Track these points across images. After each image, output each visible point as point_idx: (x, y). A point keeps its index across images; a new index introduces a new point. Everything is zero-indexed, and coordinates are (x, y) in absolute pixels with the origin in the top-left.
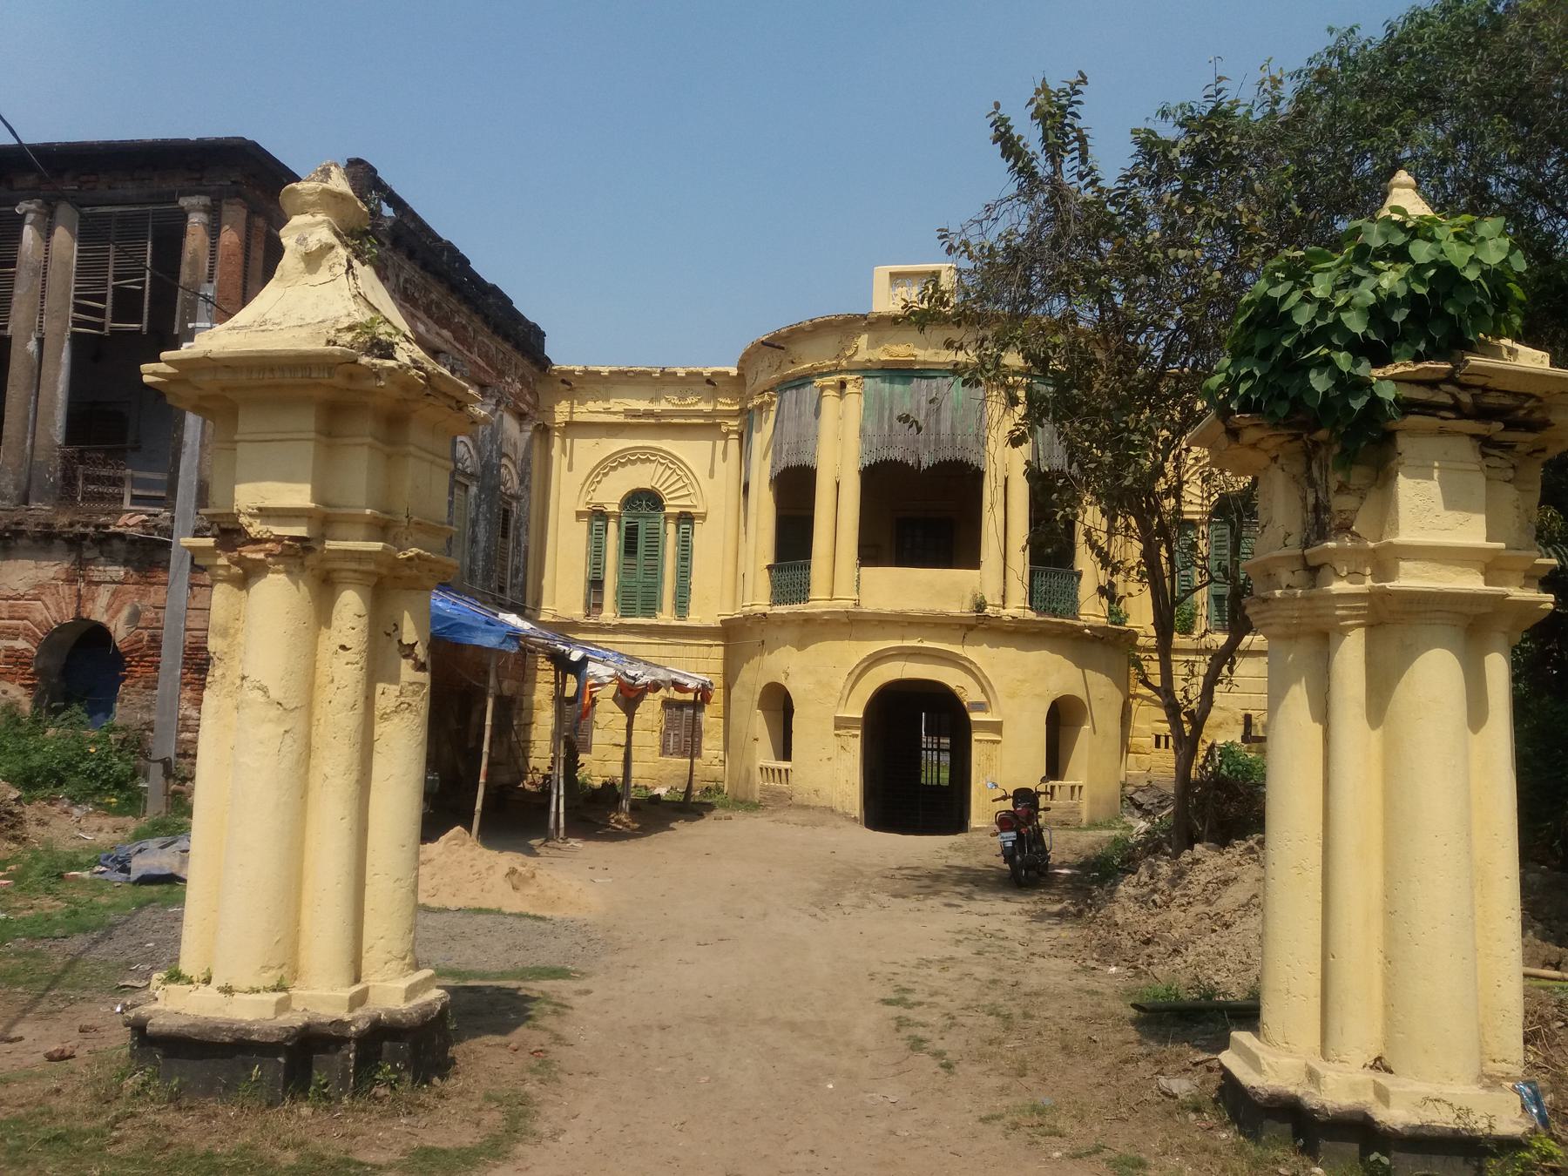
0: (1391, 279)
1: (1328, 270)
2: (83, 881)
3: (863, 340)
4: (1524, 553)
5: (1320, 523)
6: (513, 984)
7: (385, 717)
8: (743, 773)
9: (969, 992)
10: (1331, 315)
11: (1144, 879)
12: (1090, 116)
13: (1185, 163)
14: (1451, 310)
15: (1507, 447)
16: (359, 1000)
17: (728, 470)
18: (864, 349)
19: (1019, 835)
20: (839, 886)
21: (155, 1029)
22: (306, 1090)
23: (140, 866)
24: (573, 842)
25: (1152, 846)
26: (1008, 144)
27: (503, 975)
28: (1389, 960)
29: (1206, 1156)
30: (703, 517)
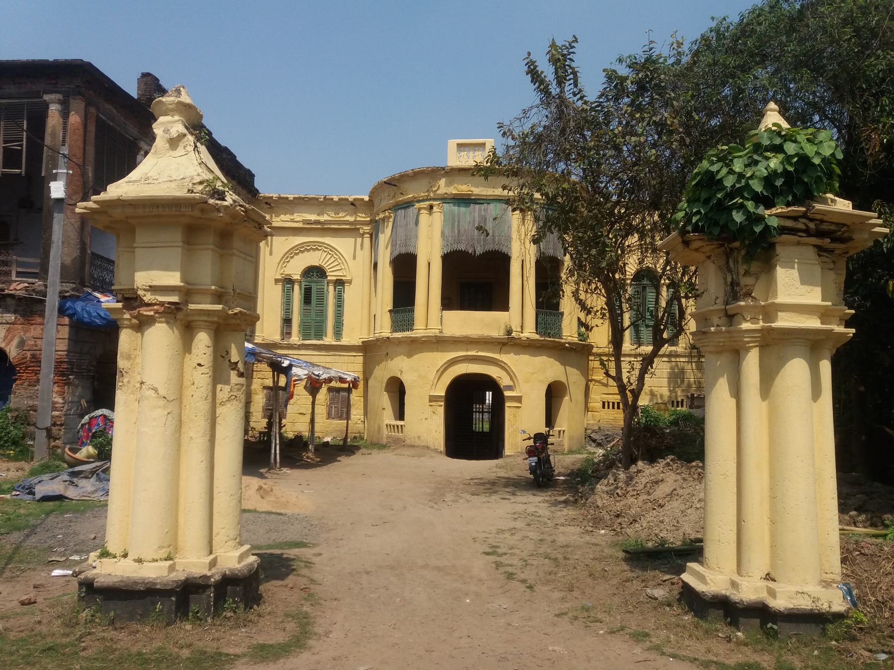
0: (775, 163)
1: (740, 157)
2: (7, 501)
3: (442, 182)
4: (839, 307)
5: (734, 292)
6: (278, 552)
7: (222, 404)
8: (376, 428)
9: (530, 547)
10: (743, 181)
11: (612, 481)
12: (580, 61)
13: (631, 87)
14: (806, 180)
15: (831, 251)
16: (213, 564)
17: (364, 255)
18: (443, 187)
19: (539, 459)
20: (440, 491)
21: (99, 584)
22: (187, 615)
23: (41, 490)
24: (285, 470)
25: (609, 464)
26: (535, 75)
27: (269, 547)
28: (773, 522)
29: (679, 629)
30: (350, 282)
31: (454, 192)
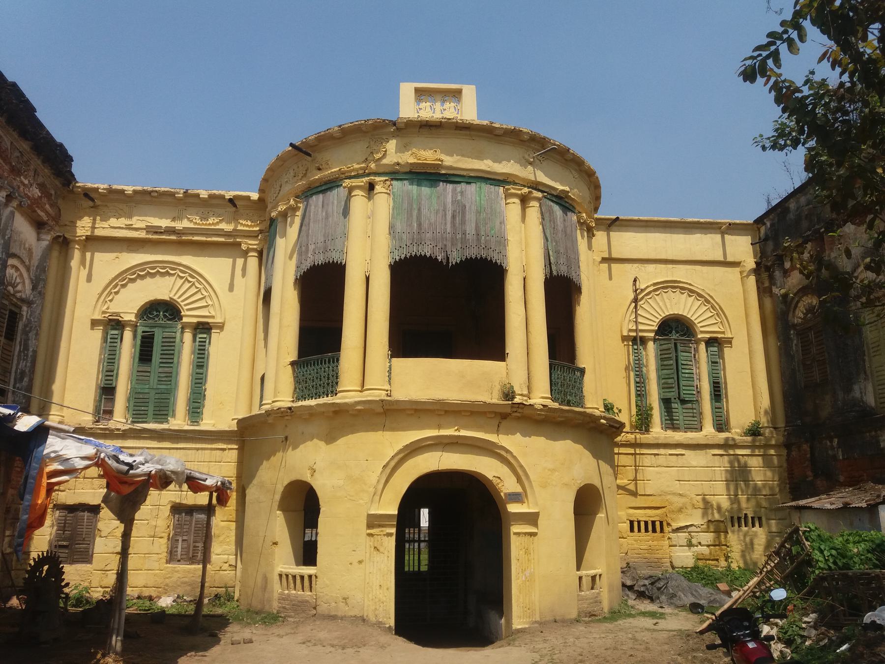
3: (391, 145)
18: (393, 153)
30: (221, 327)
31: (412, 160)
